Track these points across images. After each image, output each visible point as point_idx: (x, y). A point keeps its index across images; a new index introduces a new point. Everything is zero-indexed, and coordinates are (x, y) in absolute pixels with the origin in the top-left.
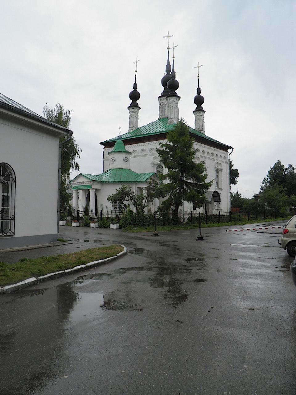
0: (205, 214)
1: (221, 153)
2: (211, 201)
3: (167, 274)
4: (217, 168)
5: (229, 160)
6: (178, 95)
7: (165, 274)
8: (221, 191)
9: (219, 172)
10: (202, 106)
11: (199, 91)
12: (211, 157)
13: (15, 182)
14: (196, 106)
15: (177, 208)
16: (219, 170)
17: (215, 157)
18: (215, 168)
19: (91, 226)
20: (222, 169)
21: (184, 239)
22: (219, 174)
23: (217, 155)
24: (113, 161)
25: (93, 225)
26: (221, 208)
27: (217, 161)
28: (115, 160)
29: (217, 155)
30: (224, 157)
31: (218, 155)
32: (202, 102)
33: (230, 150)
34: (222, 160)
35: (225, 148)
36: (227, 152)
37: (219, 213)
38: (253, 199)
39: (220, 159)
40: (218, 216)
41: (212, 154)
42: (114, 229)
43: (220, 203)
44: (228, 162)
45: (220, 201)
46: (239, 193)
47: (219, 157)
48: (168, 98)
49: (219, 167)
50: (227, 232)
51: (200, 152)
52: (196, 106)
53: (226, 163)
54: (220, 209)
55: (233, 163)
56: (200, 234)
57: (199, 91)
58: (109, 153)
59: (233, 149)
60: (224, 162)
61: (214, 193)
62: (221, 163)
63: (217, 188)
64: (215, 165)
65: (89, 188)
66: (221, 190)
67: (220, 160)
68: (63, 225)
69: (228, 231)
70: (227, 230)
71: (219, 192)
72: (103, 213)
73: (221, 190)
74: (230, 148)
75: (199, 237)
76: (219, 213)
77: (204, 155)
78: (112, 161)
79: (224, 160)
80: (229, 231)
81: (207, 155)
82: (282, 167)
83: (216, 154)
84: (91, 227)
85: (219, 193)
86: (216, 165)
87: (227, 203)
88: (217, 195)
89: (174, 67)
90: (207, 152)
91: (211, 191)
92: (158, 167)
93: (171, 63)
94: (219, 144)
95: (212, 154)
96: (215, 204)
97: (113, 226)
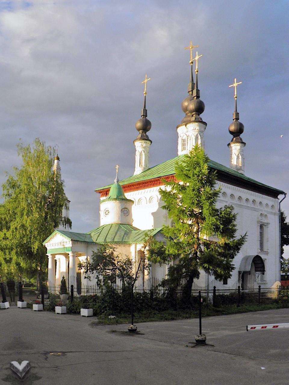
0: (237, 292)
1: (267, 200)
2: (249, 270)
4: (261, 222)
5: (280, 210)
6: (203, 121)
8: (266, 256)
9: (264, 227)
12: (252, 206)
15: (190, 282)
16: (264, 225)
17: (257, 206)
18: (258, 222)
19: (56, 310)
20: (268, 224)
22: (264, 230)
23: (260, 203)
24: (107, 213)
25: (58, 309)
26: (239, 287)
27: (261, 212)
28: (109, 212)
29: (260, 203)
30: (272, 206)
31: (263, 203)
33: (281, 197)
34: (268, 210)
35: (274, 193)
36: (277, 199)
39: (266, 209)
40: (257, 293)
41: (254, 201)
42: (85, 316)
43: (263, 274)
44: (278, 213)
45: (264, 271)
47: (265, 206)
48: (188, 125)
49: (265, 221)
50: (247, 330)
51: (235, 198)
53: (275, 214)
54: (264, 282)
55: (286, 214)
56: (201, 333)
59: (285, 194)
60: (271, 213)
61: (254, 258)
62: (267, 214)
63: (260, 251)
64: (258, 218)
66: (267, 253)
67: (265, 210)
68: (22, 308)
69: (249, 328)
70: (248, 326)
71: (263, 257)
73: (267, 253)
74: (282, 193)
75: (197, 338)
77: (240, 202)
78: (105, 213)
79: (271, 211)
80: (252, 328)
81: (259, 206)
83: (267, 204)
84: (56, 312)
85: (262, 258)
86: (260, 218)
87: (276, 274)
88: (259, 262)
89: (198, 82)
90: (245, 199)
91: (250, 256)
93: (195, 82)
94: (264, 188)
95: (254, 201)
96: (257, 275)
97: (84, 312)
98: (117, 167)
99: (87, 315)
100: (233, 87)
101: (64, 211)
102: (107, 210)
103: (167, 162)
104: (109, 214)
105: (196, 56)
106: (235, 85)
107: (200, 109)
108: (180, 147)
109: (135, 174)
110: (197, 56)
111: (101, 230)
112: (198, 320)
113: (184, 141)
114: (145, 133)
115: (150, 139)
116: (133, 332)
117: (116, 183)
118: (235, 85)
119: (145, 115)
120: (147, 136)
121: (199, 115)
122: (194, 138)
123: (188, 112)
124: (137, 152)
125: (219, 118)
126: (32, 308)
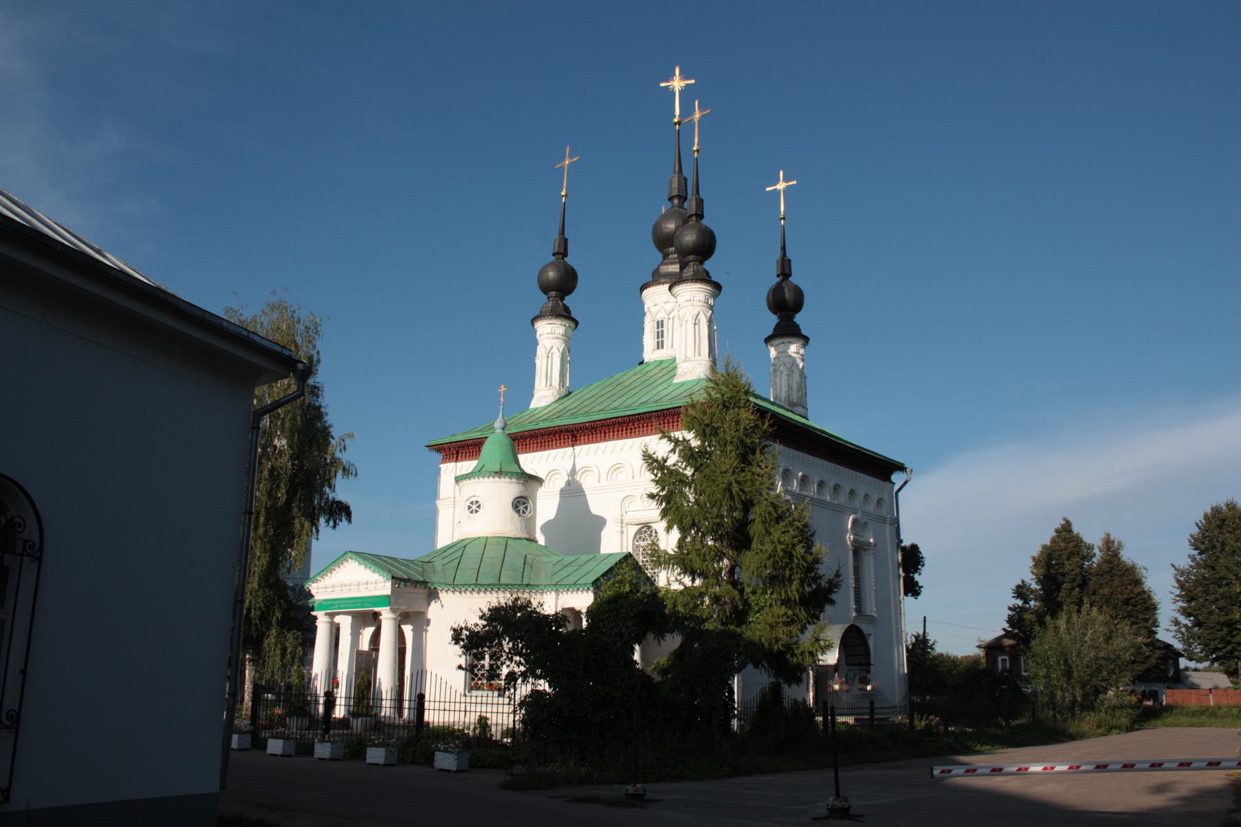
1: (865, 483)
3: (446, 751)
6: (713, 279)
7: (439, 750)
10: (799, 318)
11: (785, 270)
13: (39, 559)
14: (773, 320)
21: (421, 698)
24: (474, 507)
32: (798, 305)
33: (898, 478)
35: (882, 468)
36: (887, 484)
37: (872, 709)
38: (975, 661)
45: (869, 664)
46: (931, 637)
48: (677, 289)
52: (773, 320)
57: (785, 270)
58: (458, 479)
65: (376, 609)
71: (865, 628)
72: (427, 704)
76: (872, 709)
82: (1078, 541)
92: (639, 532)
93: (689, 173)
98: (503, 388)
99: (381, 761)
100: (777, 192)
101: (709, 626)
102: (474, 499)
103: (616, 376)
104: (480, 511)
105: (680, 92)
106: (781, 186)
107: (705, 247)
108: (649, 340)
109: (533, 405)
110: (677, 78)
111: (459, 553)
112: (830, 774)
113: (660, 324)
114: (562, 299)
115: (573, 315)
116: (638, 800)
117: (499, 431)
118: (781, 186)
119: (562, 252)
120: (567, 309)
121: (701, 263)
122: (691, 322)
123: (672, 249)
124: (539, 348)
125: (747, 264)
126: (265, 748)
